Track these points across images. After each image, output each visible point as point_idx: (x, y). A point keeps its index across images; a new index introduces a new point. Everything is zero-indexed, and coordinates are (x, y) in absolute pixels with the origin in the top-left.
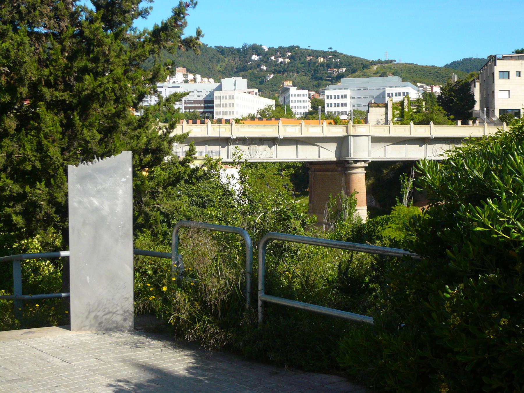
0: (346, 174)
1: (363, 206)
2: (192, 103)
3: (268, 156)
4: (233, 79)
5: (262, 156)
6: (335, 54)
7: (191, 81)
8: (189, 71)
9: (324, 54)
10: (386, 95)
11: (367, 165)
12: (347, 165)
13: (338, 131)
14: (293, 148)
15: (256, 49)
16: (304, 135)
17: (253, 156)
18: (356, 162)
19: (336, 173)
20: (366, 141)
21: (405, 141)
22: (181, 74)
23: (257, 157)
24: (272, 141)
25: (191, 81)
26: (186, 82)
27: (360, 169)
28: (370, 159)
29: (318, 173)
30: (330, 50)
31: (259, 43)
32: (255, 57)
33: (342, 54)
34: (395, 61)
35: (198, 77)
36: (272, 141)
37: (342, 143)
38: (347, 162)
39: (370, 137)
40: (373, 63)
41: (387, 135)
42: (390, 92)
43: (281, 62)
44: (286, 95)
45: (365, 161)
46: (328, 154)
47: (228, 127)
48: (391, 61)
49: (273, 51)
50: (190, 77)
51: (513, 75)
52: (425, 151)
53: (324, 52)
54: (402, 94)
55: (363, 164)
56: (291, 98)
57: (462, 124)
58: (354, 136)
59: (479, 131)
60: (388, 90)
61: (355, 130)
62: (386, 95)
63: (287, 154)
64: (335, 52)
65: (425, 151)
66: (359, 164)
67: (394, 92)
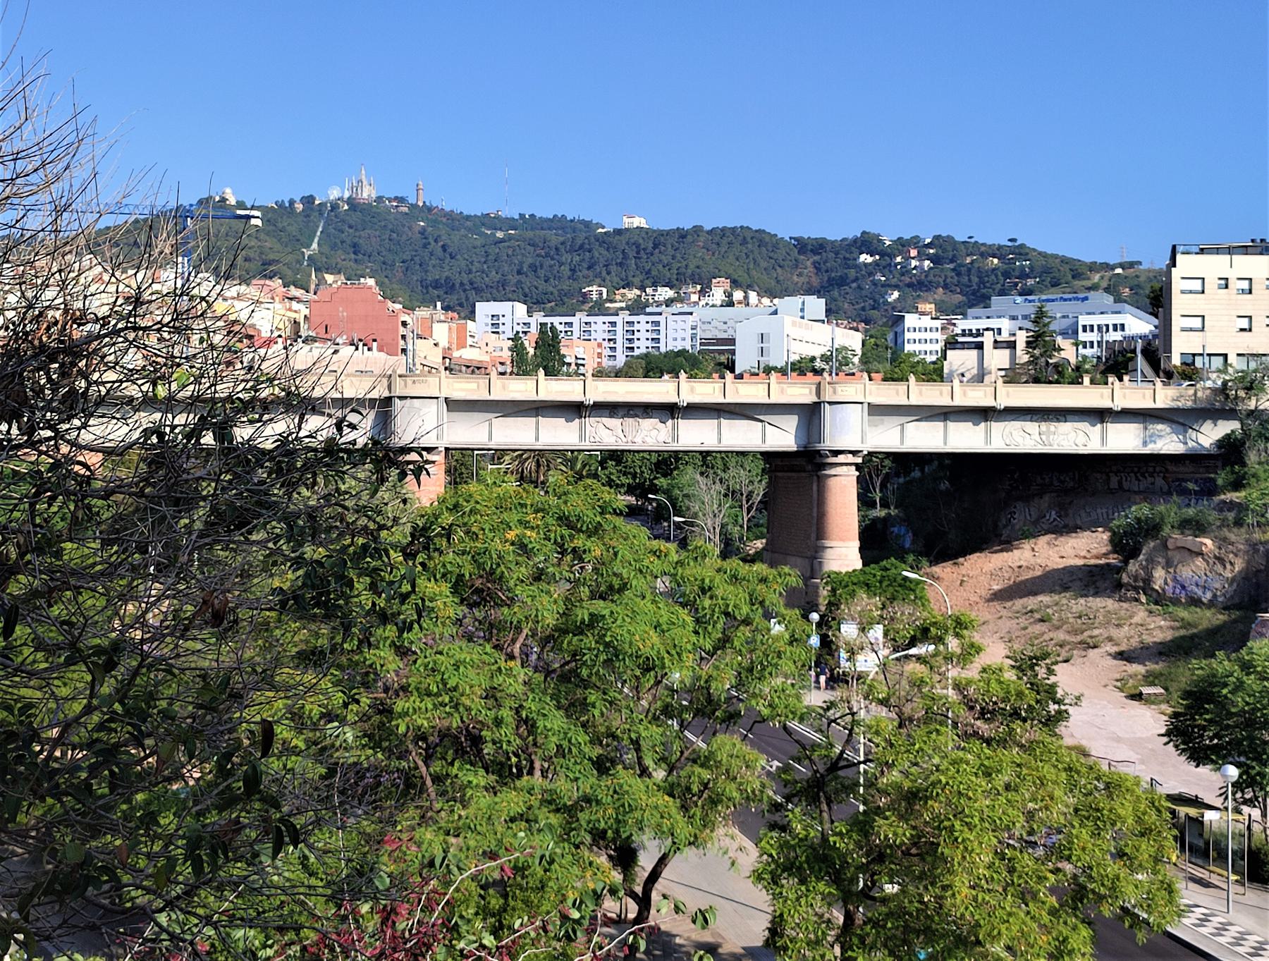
0: (818, 477)
1: (850, 540)
2: (713, 344)
3: (661, 439)
4: (798, 300)
5: (648, 440)
6: (1021, 251)
7: (740, 303)
8: (735, 284)
9: (998, 252)
10: (1080, 329)
11: (859, 460)
12: (818, 460)
13: (800, 392)
14: (1032, 427)
15: (866, 243)
16: (728, 400)
17: (630, 439)
18: (836, 453)
19: (803, 474)
20: (855, 415)
21: (537, 409)
22: (721, 290)
23: (638, 440)
24: (669, 411)
25: (740, 303)
26: (730, 304)
27: (845, 468)
28: (866, 448)
29: (780, 474)
30: (1010, 244)
31: (873, 230)
32: (865, 258)
33: (1034, 250)
34: (1140, 263)
35: (753, 296)
36: (669, 411)
37: (811, 415)
38: (818, 452)
39: (866, 406)
40: (1093, 267)
41: (483, 395)
42: (1087, 323)
43: (915, 268)
44: (898, 330)
45: (854, 453)
46: (782, 436)
47: (483, 382)
48: (1132, 265)
49: (902, 245)
50: (738, 295)
51: (1212, 284)
52: (988, 433)
53: (1000, 247)
54: (1096, 328)
55: (850, 458)
56: (908, 335)
57: (1092, 382)
58: (830, 403)
59: (1102, 396)
60: (1084, 320)
61: (835, 392)
62: (1080, 329)
63: (607, 434)
64: (1022, 246)
65: (988, 433)
66: (841, 459)
67: (1110, 323)
